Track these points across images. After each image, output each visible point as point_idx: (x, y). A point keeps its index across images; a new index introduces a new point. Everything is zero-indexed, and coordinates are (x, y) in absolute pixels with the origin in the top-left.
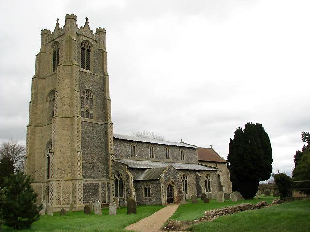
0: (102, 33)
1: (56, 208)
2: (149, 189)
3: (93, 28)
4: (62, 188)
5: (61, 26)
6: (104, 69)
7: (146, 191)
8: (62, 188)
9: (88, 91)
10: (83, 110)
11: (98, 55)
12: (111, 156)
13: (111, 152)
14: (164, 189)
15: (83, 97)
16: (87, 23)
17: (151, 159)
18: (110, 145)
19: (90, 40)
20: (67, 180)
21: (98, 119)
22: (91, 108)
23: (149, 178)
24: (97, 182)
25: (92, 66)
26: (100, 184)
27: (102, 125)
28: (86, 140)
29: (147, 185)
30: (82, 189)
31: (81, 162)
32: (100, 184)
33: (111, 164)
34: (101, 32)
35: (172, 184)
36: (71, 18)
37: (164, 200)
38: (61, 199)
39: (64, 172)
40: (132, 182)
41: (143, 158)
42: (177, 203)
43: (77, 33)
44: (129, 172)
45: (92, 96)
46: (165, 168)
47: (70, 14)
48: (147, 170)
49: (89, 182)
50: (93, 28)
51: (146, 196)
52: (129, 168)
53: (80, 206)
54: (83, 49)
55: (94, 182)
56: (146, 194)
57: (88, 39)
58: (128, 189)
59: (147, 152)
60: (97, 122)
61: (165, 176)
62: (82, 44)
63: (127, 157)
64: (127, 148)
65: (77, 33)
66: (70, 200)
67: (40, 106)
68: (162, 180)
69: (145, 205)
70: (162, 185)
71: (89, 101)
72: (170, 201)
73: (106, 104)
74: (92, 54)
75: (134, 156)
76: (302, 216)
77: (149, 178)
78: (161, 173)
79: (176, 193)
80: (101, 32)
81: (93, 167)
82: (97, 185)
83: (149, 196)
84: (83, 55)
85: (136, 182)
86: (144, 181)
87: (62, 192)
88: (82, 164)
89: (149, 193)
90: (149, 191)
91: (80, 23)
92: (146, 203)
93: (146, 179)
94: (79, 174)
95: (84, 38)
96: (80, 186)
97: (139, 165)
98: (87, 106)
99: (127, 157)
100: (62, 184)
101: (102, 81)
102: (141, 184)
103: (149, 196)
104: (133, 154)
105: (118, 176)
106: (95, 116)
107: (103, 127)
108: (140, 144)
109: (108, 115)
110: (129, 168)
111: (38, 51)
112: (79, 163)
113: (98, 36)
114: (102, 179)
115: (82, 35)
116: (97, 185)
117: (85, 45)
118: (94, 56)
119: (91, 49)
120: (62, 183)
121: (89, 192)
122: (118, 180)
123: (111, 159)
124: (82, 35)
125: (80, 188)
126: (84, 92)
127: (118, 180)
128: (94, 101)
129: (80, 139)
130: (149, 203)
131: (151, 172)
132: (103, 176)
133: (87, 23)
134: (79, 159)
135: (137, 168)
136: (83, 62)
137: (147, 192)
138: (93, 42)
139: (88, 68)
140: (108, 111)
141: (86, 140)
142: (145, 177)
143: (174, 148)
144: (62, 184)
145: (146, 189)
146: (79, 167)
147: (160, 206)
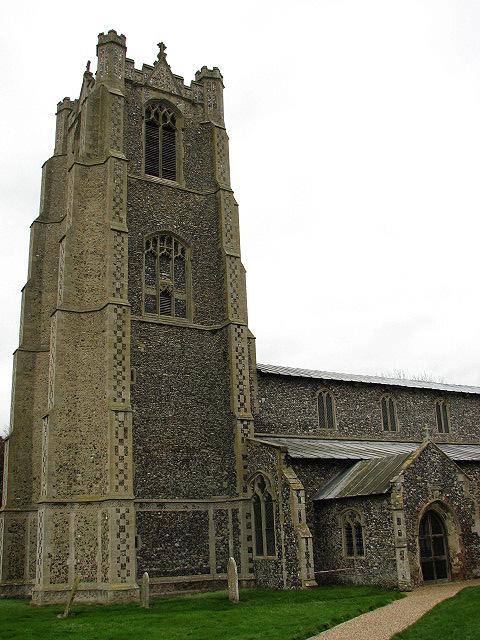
0: (211, 81)
1: (47, 593)
2: (359, 527)
3: (185, 68)
4: (72, 529)
5: (93, 69)
6: (218, 173)
7: (349, 537)
8: (72, 529)
9: (166, 237)
10: (153, 292)
11: (198, 139)
12: (240, 425)
13: (240, 414)
14: (401, 528)
15: (152, 255)
16: (162, 56)
17: (389, 435)
18: (236, 392)
19: (173, 100)
20: (89, 503)
21: (201, 316)
22: (180, 285)
23: (358, 489)
24: (202, 509)
25: (180, 169)
26: (211, 512)
27: (214, 332)
28: (160, 378)
29: (353, 516)
30: (132, 530)
31: (129, 443)
32: (211, 512)
33: (239, 448)
34: (210, 79)
35: (437, 508)
36: (111, 44)
37: (404, 569)
38: (71, 562)
39: (79, 478)
40: (299, 506)
41: (359, 430)
42: (464, 574)
43: (127, 81)
44: (290, 475)
45: (183, 252)
46: (408, 456)
47: (119, 34)
48: (358, 465)
49: (169, 508)
50: (185, 68)
51: (350, 553)
52: (293, 462)
53: (124, 586)
54: (151, 125)
55: (190, 509)
56: (350, 545)
57: (166, 97)
58: (289, 529)
59: (375, 414)
60: (198, 326)
61: (410, 481)
62: (148, 112)
63: (306, 428)
64: (306, 405)
65: (127, 81)
66: (95, 567)
67: (49, 297)
68: (398, 497)
69: (350, 582)
70: (397, 515)
71: (172, 264)
72: (433, 570)
73: (224, 271)
74: (180, 136)
75: (331, 425)
76: (287, 426)
77: (358, 489)
78: (395, 473)
79: (454, 542)
80: (210, 79)
81: (186, 461)
82: (200, 519)
83: (361, 553)
84: (151, 141)
85: (318, 509)
86: (341, 501)
87: (73, 540)
88: (130, 451)
89: (360, 544)
90: (359, 536)
91: (141, 54)
92: (353, 578)
93: (347, 495)
94: (122, 483)
95: (153, 95)
96: (123, 523)
97: (330, 449)
98: (166, 280)
99: (306, 428)
100: (73, 515)
101: (212, 208)
102: (335, 511)
103: (361, 553)
104: (326, 420)
105: (262, 486)
106: (192, 306)
107: (217, 338)
108: (350, 391)
109: (230, 300)
110: (293, 462)
111: (48, 151)
112: (121, 449)
113: (198, 89)
114: (218, 498)
115: (146, 86)
116: (200, 519)
117: (156, 114)
118: (187, 141)
119: (179, 124)
120: (73, 514)
121: (170, 540)
122: (263, 499)
123: (240, 435)
124: (146, 86)
125: (122, 529)
126: (155, 241)
127: (263, 499)
128: (189, 265)
129: (127, 374)
130: (358, 578)
131: (367, 471)
132: (221, 491)
133: (162, 56)
134: (121, 436)
135: (318, 461)
136: (151, 158)
137: (355, 542)
138: (181, 106)
139: (170, 174)
140: (230, 290)
141: (160, 378)
142: (348, 488)
143: (462, 401)
144: (73, 515)
145: (349, 529)
146: (122, 459)
147: (395, 592)
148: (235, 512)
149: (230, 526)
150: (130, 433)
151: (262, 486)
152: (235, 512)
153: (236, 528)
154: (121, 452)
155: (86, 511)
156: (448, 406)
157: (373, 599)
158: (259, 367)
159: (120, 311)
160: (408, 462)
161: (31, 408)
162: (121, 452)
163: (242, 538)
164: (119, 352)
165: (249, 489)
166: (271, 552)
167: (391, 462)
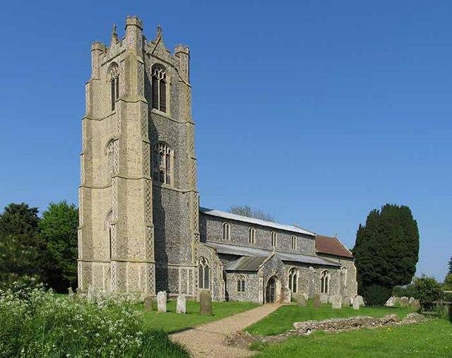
2: (243, 282)
19: (165, 65)
32: (180, 271)
38: (127, 284)
51: (239, 290)
74: (168, 86)
83: (243, 291)
89: (243, 288)
90: (243, 285)
95: (156, 61)
100: (127, 266)
103: (243, 291)
105: (204, 262)
122: (204, 267)
125: (151, 274)
127: (204, 267)
145: (239, 282)
146: (150, 246)
148: (190, 271)
149: (188, 276)
150: (153, 236)
151: (204, 262)
152: (190, 271)
153: (191, 277)
154: (150, 244)
155: (133, 265)
156: (255, 231)
157: (241, 309)
158: (446, 281)
159: (148, 181)
160: (266, 260)
161: (91, 214)
162: (150, 244)
163: (193, 281)
164: (148, 200)
165: (197, 262)
166: (207, 287)
167: (258, 259)
